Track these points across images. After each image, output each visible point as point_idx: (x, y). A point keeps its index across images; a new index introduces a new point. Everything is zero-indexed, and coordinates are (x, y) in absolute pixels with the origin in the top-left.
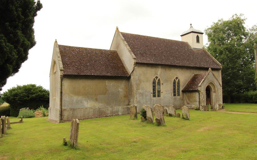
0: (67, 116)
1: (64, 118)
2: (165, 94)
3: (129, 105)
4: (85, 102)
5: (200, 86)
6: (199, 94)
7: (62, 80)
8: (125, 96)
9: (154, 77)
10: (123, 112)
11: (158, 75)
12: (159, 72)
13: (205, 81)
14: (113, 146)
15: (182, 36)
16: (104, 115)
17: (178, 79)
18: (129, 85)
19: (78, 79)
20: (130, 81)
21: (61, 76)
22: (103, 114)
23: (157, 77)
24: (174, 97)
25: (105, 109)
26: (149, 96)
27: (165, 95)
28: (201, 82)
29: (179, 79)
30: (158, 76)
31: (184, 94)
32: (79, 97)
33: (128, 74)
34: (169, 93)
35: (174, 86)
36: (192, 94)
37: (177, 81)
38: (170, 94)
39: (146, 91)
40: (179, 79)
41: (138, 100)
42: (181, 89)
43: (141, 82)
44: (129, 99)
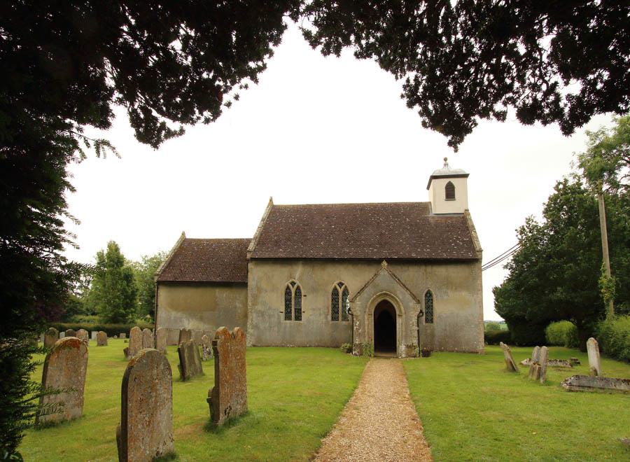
2: (311, 315)
12: (299, 272)
14: (578, 367)
17: (343, 287)
23: (293, 283)
24: (331, 322)
26: (276, 316)
29: (346, 287)
38: (323, 317)
39: (270, 308)
40: (346, 287)
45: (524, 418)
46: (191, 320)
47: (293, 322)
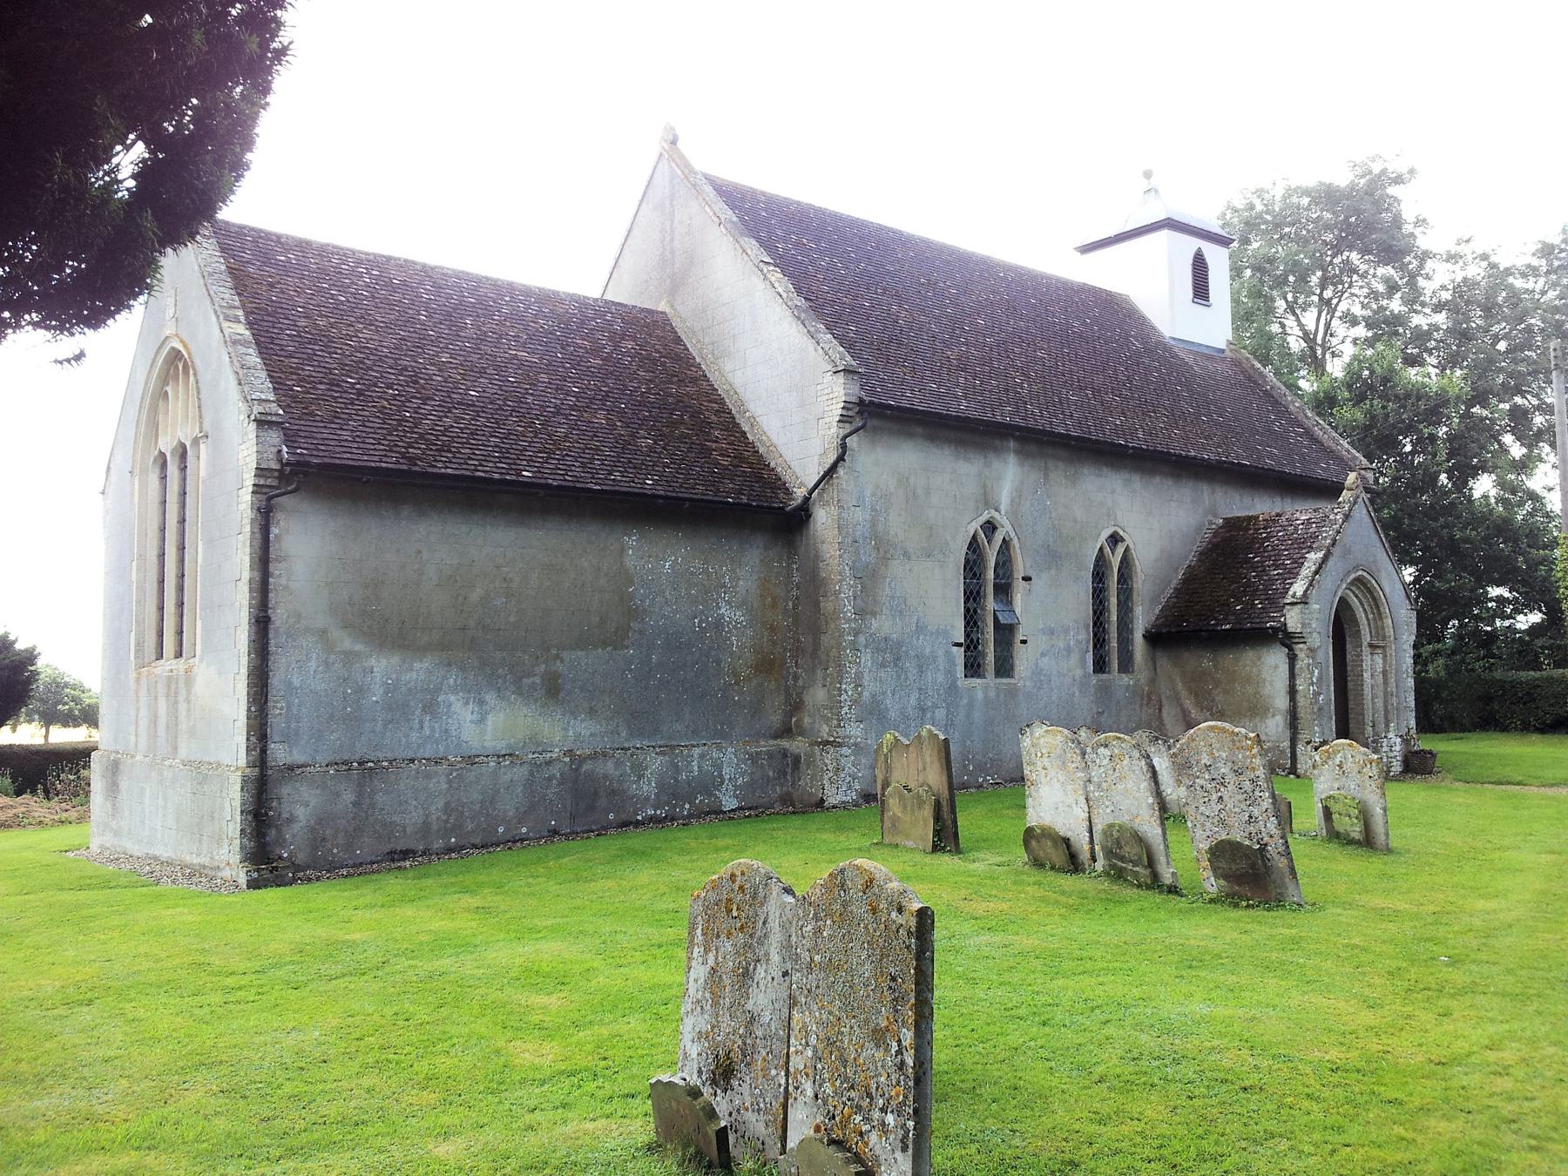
0: (312, 830)
1: (282, 843)
2: (1043, 655)
3: (786, 731)
4: (457, 706)
5: (1304, 601)
6: (1292, 659)
7: (265, 516)
8: (767, 665)
9: (975, 526)
10: (751, 785)
13: (1331, 563)
15: (1087, 249)
16: (611, 816)
17: (1120, 549)
18: (789, 575)
19: (406, 510)
20: (802, 550)
21: (260, 471)
22: (602, 802)
23: (990, 527)
24: (1094, 680)
25: (618, 764)
26: (941, 660)
27: (1045, 660)
28: (1307, 570)
29: (1127, 550)
31: (1164, 662)
32: (417, 665)
33: (788, 492)
35: (1099, 595)
36: (1228, 658)
38: (1075, 657)
39: (920, 629)
40: (1127, 550)
41: (866, 694)
42: (1142, 619)
43: (885, 559)
44: (787, 689)
45: (1440, 1130)
46: (491, 698)
47: (990, 679)
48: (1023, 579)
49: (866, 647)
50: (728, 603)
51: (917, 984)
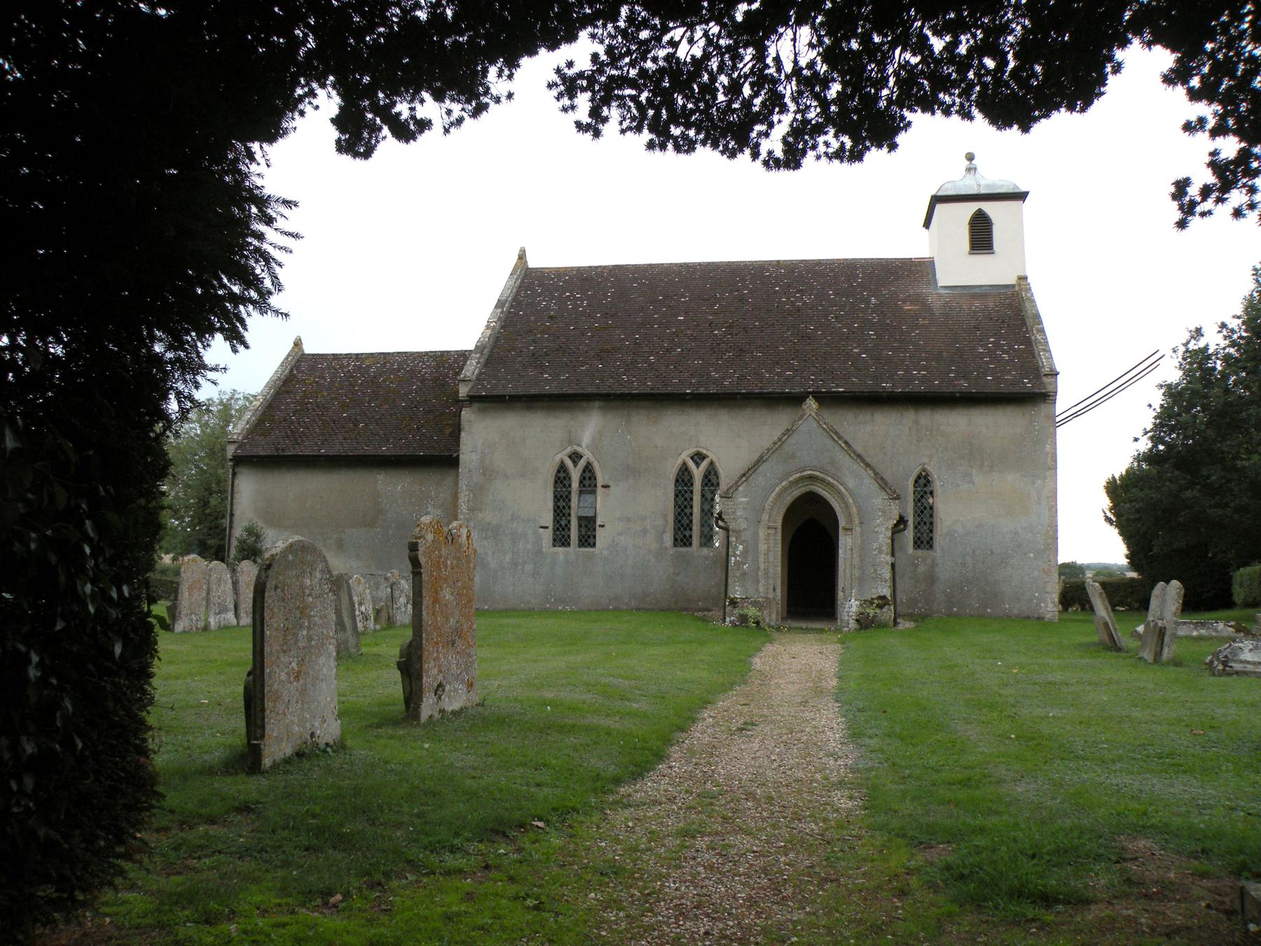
11: (579, 445)
15: (927, 224)
17: (704, 464)
23: (575, 457)
29: (712, 463)
30: (579, 449)
34: (645, 532)
37: (698, 473)
39: (514, 518)
48: (602, 486)
49: (474, 528)
50: (434, 505)
51: (660, 757)
